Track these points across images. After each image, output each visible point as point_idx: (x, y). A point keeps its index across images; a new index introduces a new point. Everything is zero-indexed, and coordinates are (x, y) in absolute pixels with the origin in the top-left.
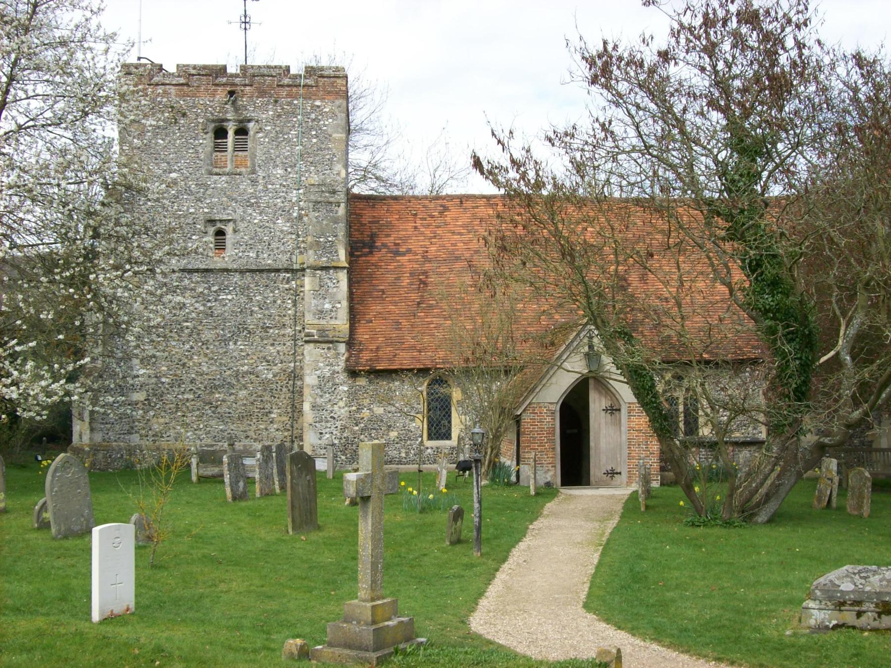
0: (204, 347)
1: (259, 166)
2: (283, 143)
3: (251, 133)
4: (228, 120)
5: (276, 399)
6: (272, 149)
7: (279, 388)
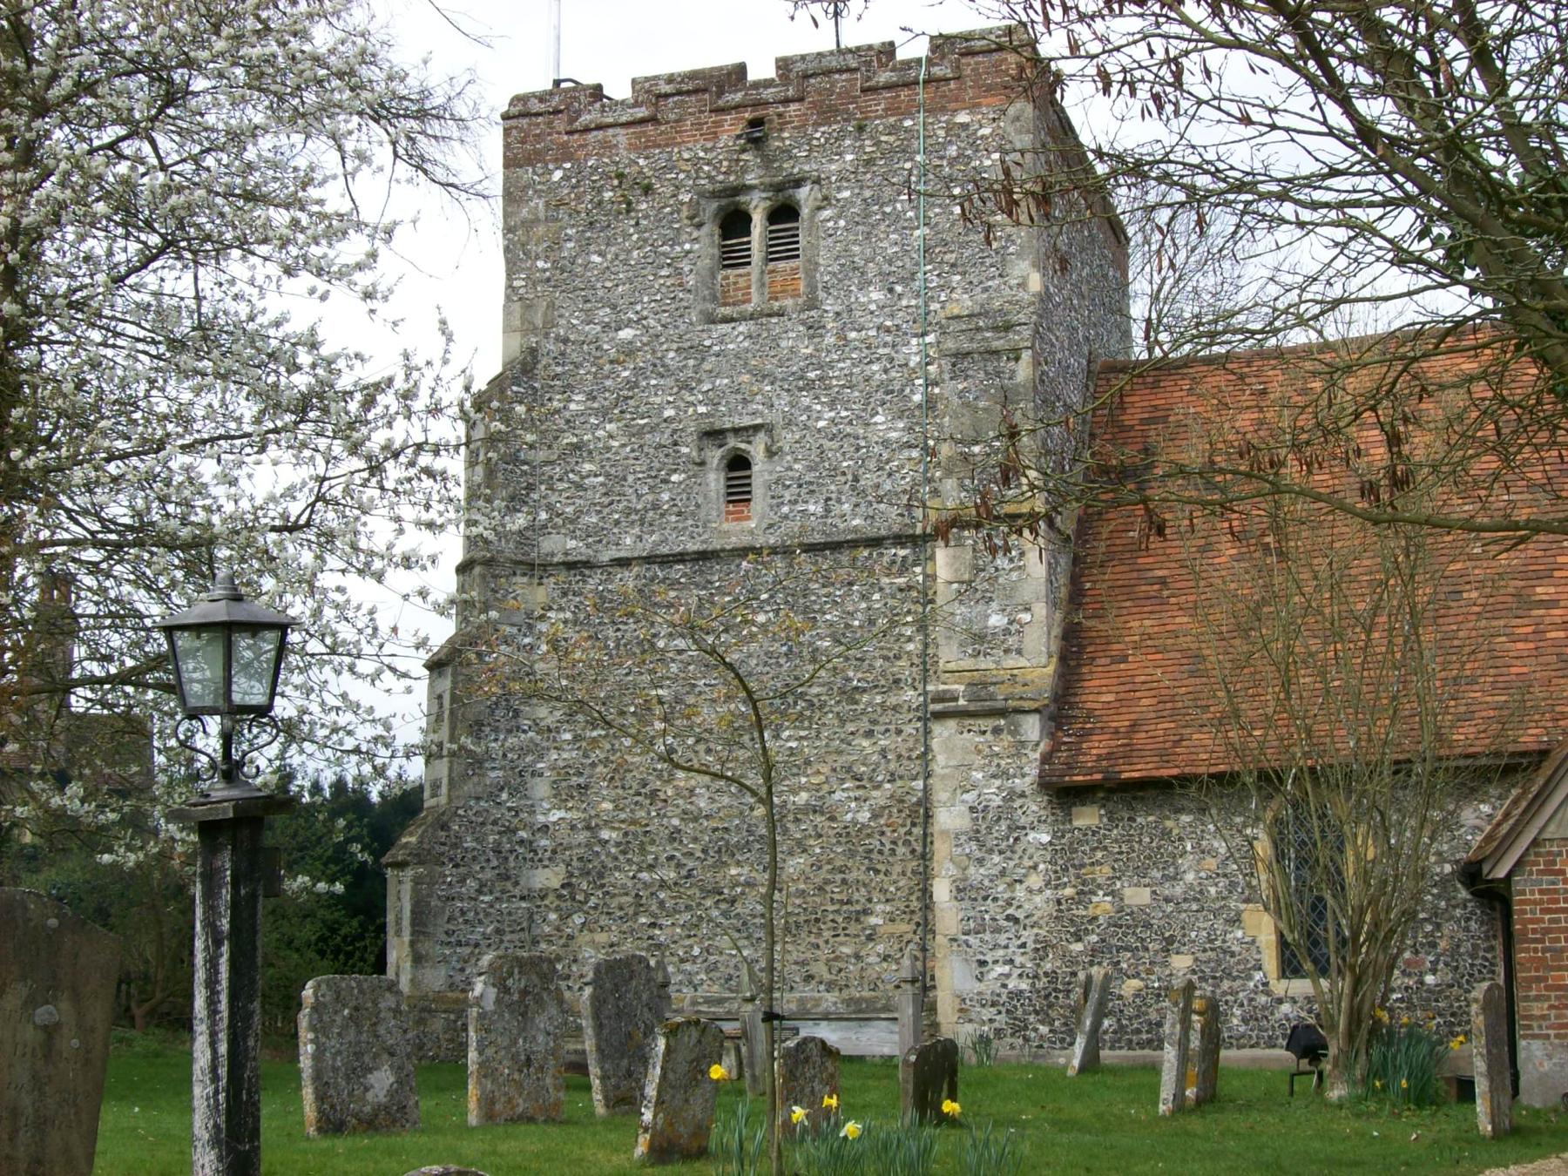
0: (701, 747)
1: (826, 289)
2: (882, 228)
3: (805, 212)
4: (748, 189)
5: (881, 876)
6: (855, 242)
7: (888, 846)
